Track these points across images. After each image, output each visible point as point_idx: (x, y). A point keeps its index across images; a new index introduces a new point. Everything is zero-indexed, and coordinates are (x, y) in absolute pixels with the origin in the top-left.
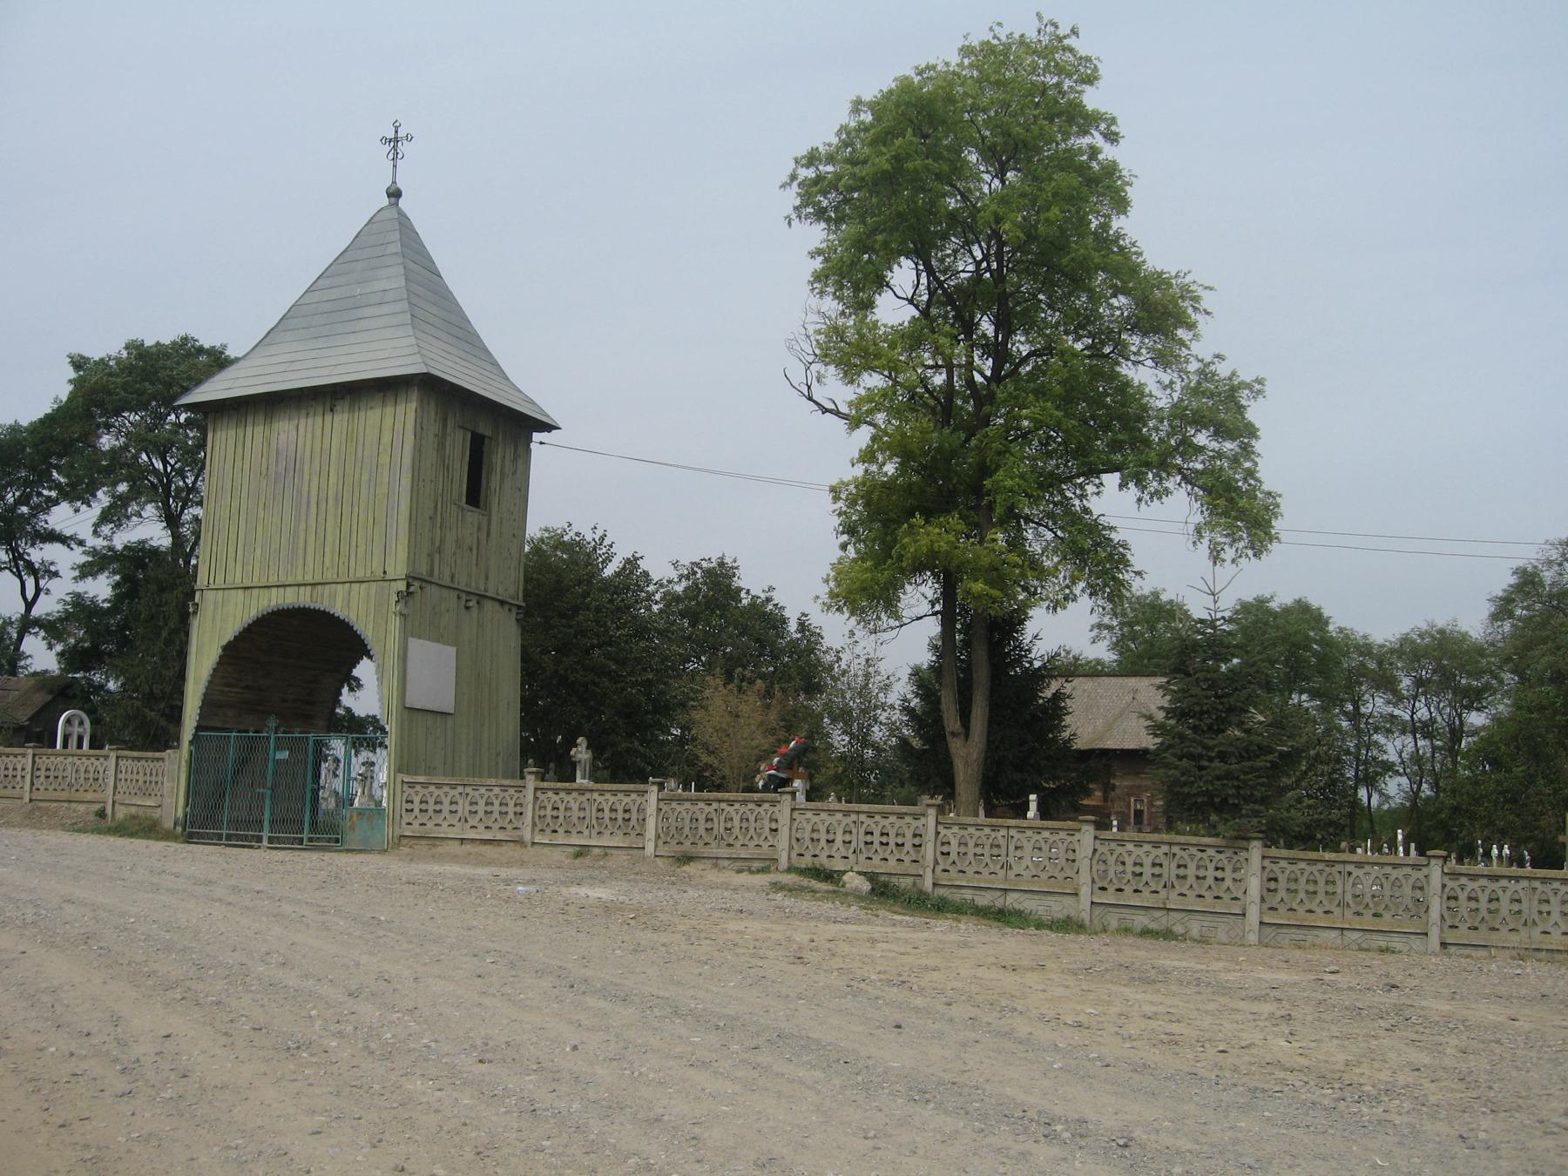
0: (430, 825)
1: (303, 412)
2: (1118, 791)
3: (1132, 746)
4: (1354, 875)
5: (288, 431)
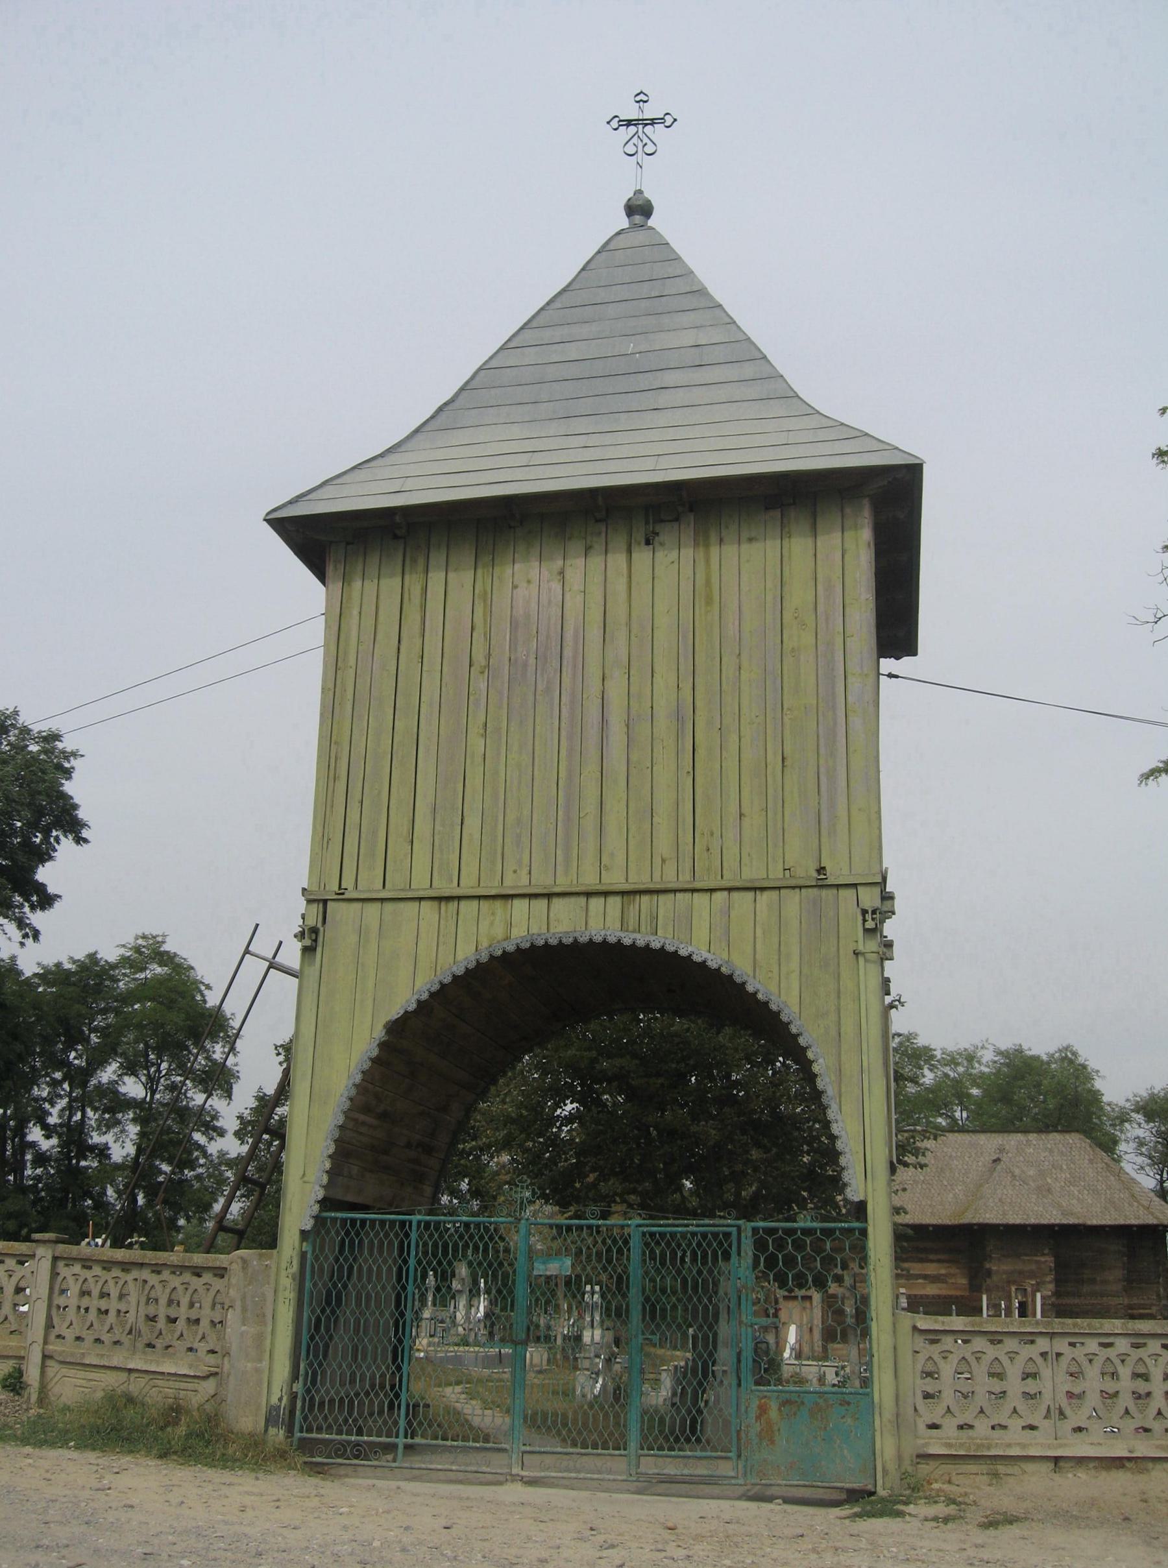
0: (982, 1428)
1: (576, 546)
2: (995, 1278)
3: (1018, 1222)
4: (150, 1283)
5: (538, 585)
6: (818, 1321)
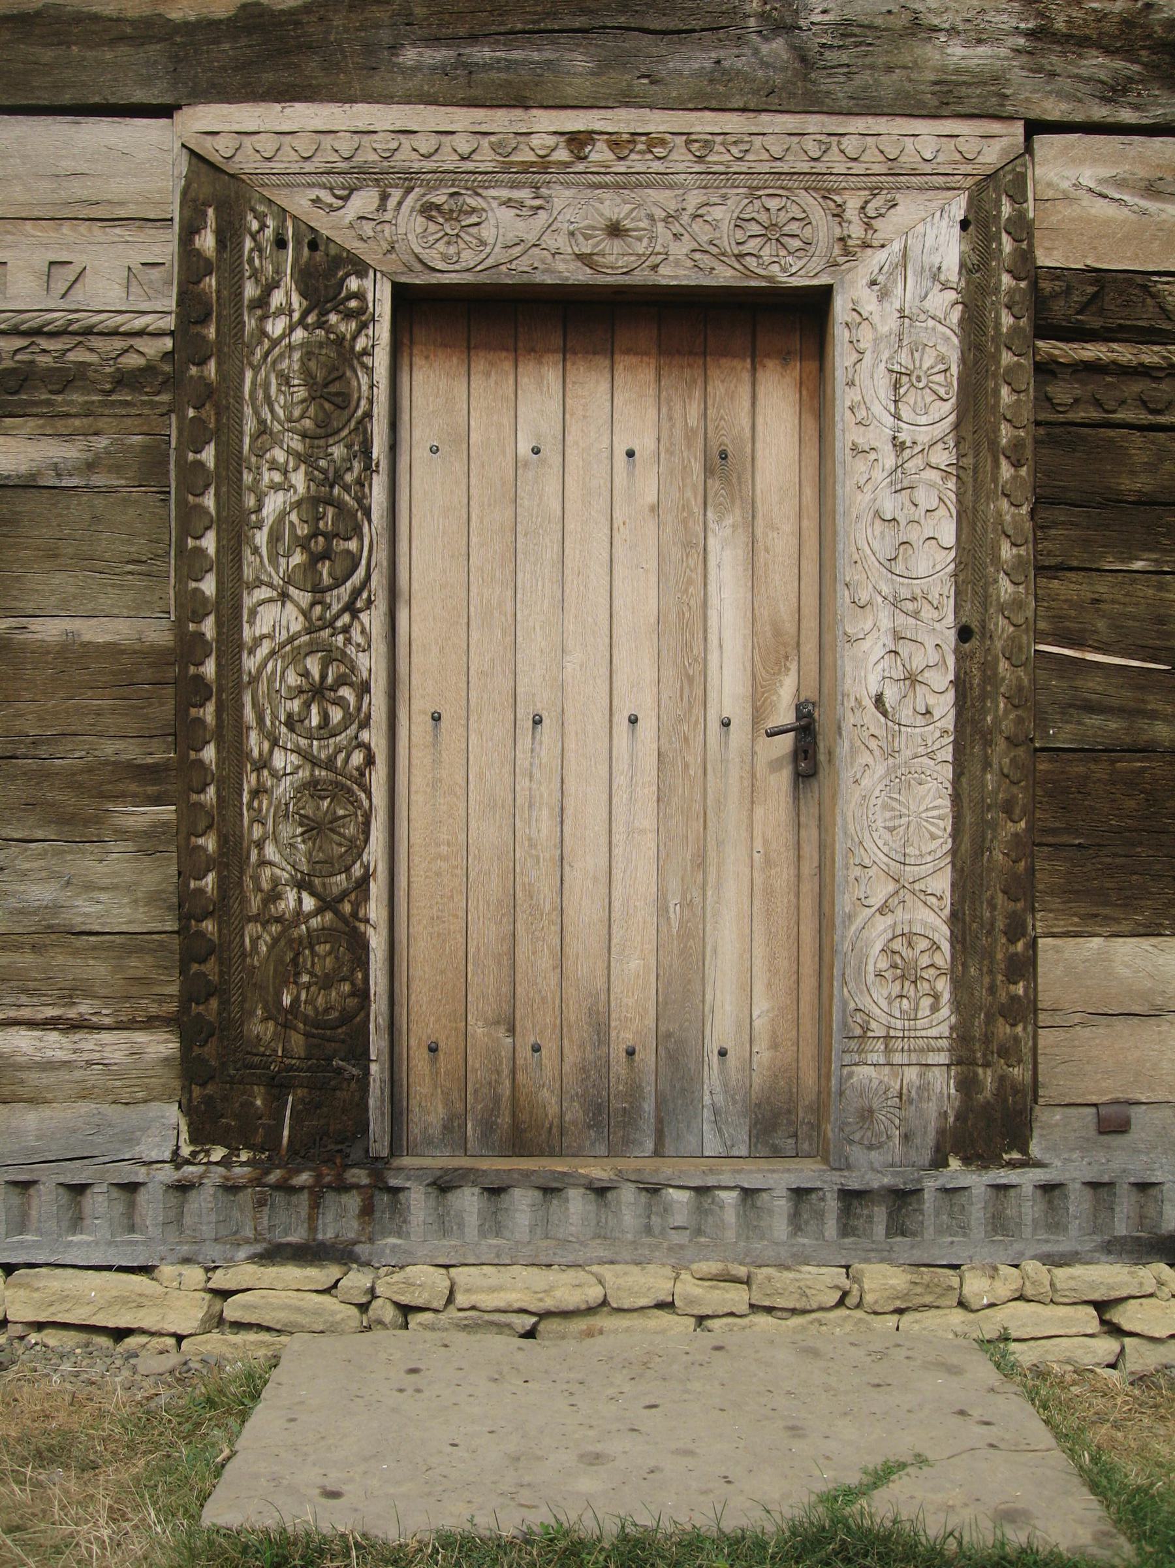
6: (900, 665)
